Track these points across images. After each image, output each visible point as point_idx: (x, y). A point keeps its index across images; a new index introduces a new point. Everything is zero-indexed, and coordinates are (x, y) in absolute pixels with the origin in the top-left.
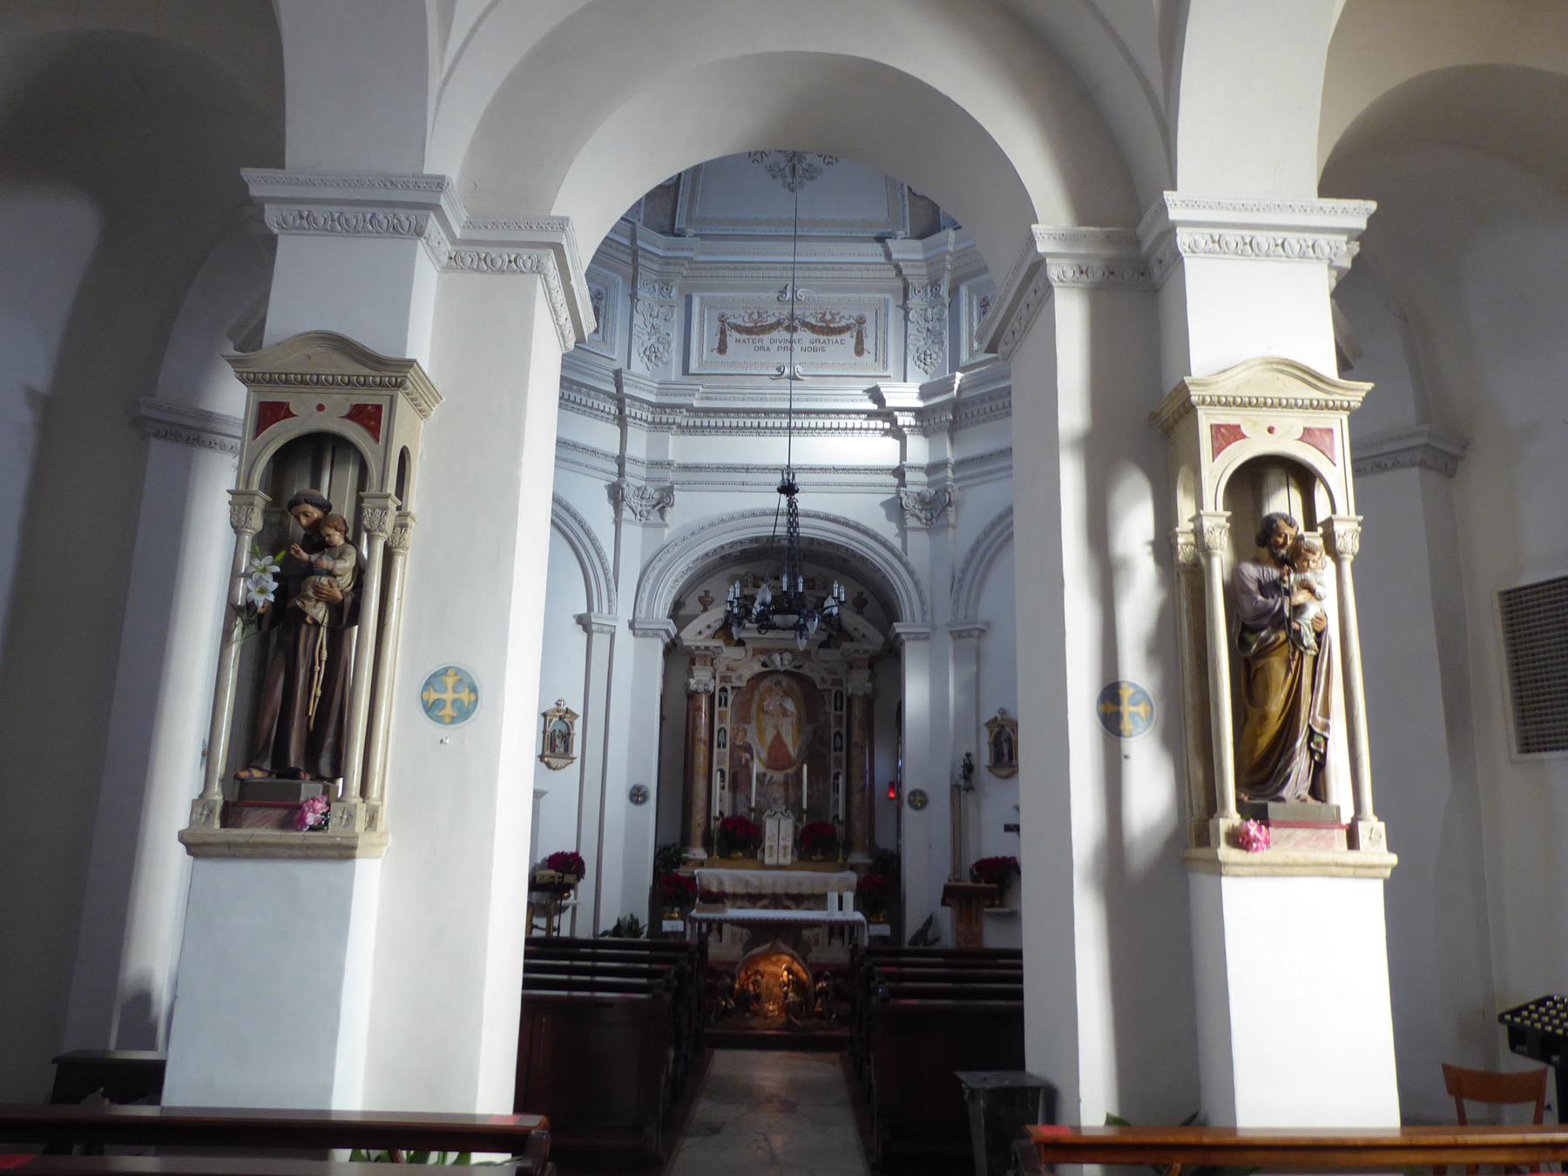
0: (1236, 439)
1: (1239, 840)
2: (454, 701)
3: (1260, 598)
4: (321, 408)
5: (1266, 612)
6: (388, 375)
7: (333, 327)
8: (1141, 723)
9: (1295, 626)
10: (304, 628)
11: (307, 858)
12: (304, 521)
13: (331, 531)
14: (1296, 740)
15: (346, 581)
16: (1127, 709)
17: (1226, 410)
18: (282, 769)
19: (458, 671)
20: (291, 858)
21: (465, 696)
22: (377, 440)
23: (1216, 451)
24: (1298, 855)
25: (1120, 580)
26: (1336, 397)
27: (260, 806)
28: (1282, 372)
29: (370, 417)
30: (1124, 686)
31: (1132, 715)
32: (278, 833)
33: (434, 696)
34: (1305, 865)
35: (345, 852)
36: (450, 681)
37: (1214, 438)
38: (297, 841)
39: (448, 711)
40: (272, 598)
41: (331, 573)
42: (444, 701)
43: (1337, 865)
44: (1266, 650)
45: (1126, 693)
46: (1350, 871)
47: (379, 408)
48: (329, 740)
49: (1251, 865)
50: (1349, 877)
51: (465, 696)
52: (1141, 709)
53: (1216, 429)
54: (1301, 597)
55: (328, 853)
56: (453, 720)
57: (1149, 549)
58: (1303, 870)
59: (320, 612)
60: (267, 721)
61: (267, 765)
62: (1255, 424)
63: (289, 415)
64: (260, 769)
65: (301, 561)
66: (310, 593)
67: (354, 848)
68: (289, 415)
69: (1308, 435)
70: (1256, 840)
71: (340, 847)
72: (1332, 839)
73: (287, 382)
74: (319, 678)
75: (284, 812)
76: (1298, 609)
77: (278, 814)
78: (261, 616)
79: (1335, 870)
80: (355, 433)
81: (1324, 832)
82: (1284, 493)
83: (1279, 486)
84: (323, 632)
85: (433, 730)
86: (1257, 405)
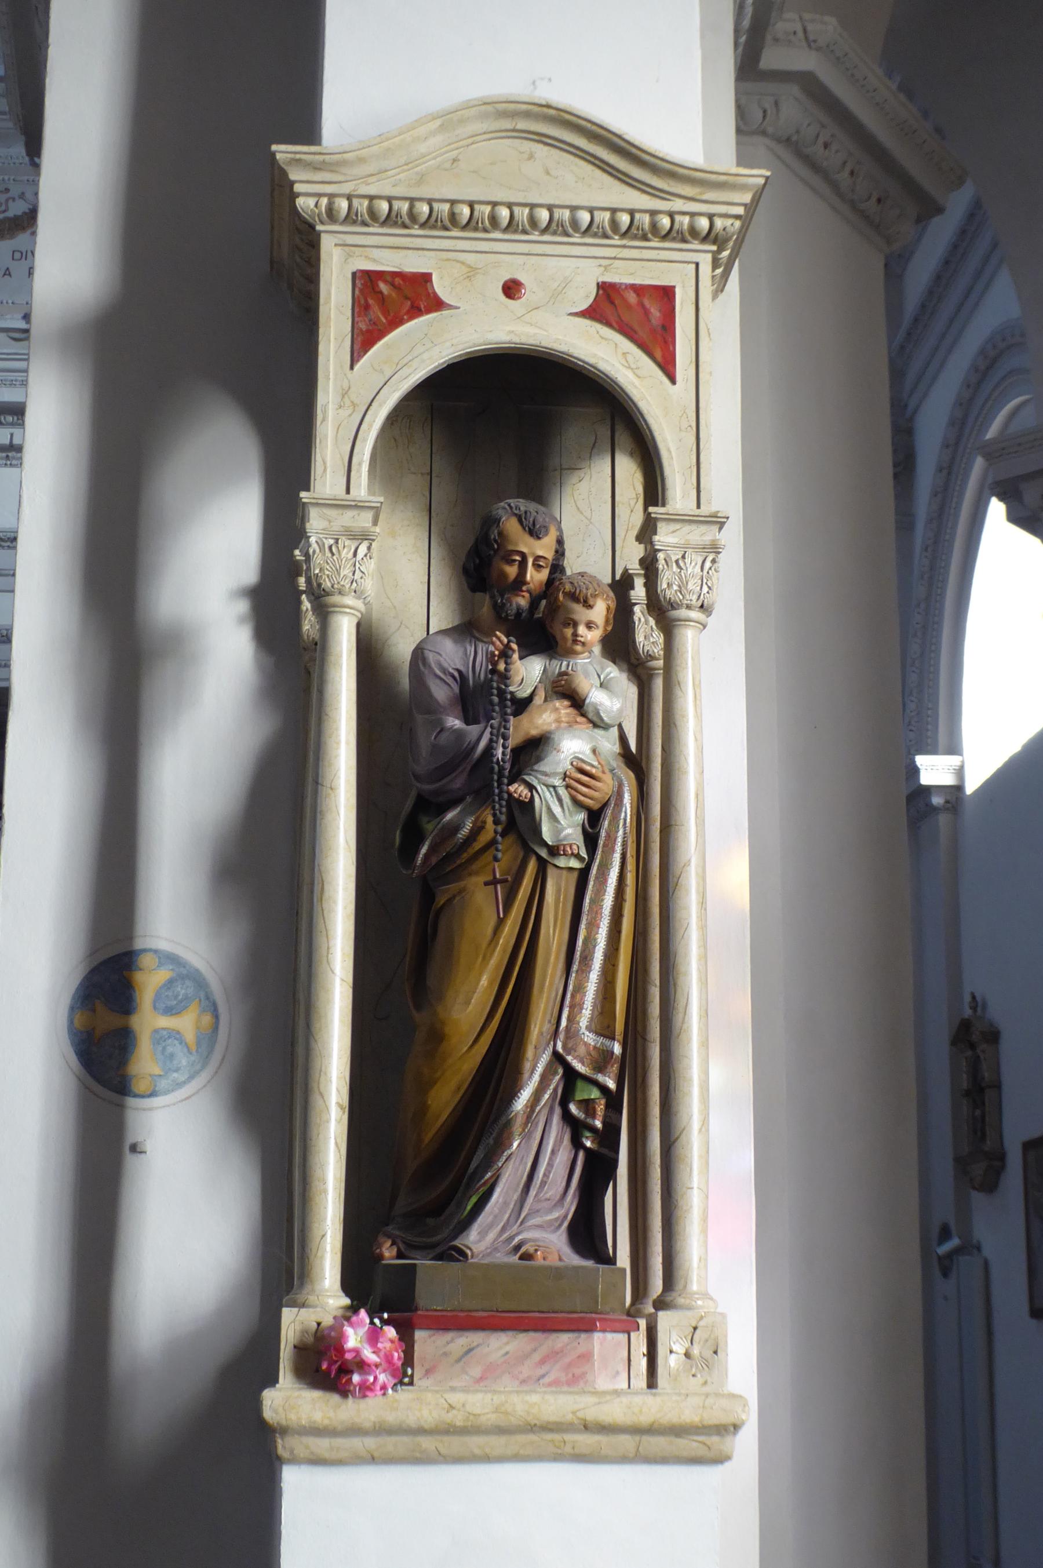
0: (416, 312)
1: (326, 1366)
3: (455, 723)
5: (458, 756)
8: (183, 1060)
9: (518, 790)
14: (513, 1094)
16: (149, 1021)
17: (394, 236)
23: (364, 340)
24: (478, 1403)
25: (158, 688)
26: (678, 205)
28: (542, 139)
30: (146, 961)
31: (160, 1037)
34: (501, 1430)
37: (360, 307)
43: (587, 1427)
44: (455, 860)
45: (151, 980)
46: (626, 1442)
47: (667, 294)
49: (354, 1431)
50: (624, 1459)
52: (187, 1023)
53: (367, 283)
54: (546, 716)
57: (243, 606)
58: (496, 1444)
62: (472, 272)
69: (609, 305)
70: (362, 1365)
72: (586, 1357)
76: (534, 748)
79: (586, 1441)
81: (564, 1338)
82: (601, 467)
83: (592, 451)
86: (471, 224)
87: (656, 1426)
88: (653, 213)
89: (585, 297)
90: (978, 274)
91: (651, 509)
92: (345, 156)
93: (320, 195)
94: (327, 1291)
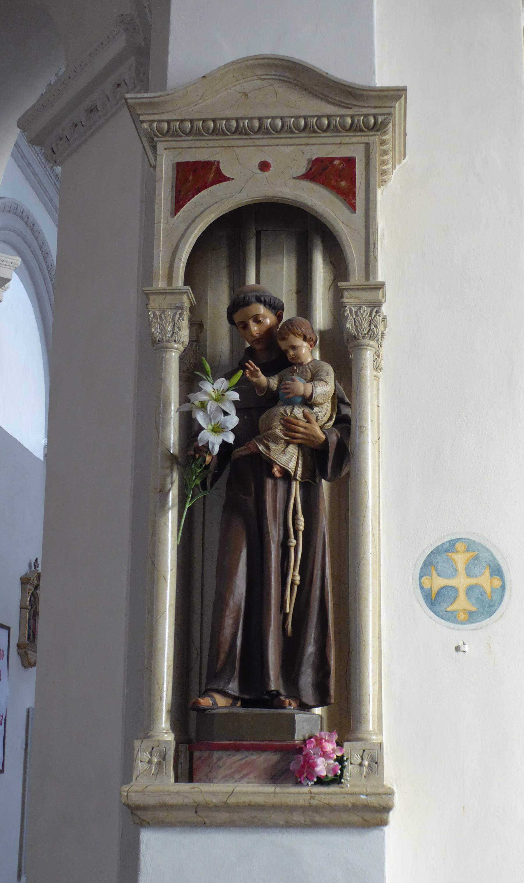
2: (470, 589)
4: (264, 166)
6: (362, 112)
7: (266, 49)
10: (269, 483)
11: (314, 825)
12: (254, 328)
13: (299, 342)
15: (324, 411)
18: (256, 694)
19: (470, 545)
20: (289, 826)
21: (484, 580)
22: (353, 207)
23: (179, 201)
27: (237, 749)
29: (338, 176)
32: (270, 789)
33: (438, 582)
35: (372, 815)
36: (460, 559)
38: (301, 801)
39: (462, 603)
40: (231, 438)
41: (308, 402)
42: (454, 589)
47: (350, 162)
48: (311, 649)
51: (484, 580)
55: (345, 817)
56: (472, 617)
59: (289, 458)
60: (228, 622)
61: (233, 687)
63: (221, 178)
64: (224, 693)
65: (257, 386)
66: (279, 431)
67: (387, 809)
68: (221, 178)
71: (367, 808)
73: (216, 131)
74: (296, 557)
75: (272, 758)
77: (265, 760)
78: (207, 467)
80: (320, 200)
84: (296, 488)
85: (449, 633)
87: (252, 803)
88: (342, 116)
89: (302, 169)
90: (29, 165)
91: (340, 284)
92: (163, 98)
93: (153, 121)
94: (371, 731)
